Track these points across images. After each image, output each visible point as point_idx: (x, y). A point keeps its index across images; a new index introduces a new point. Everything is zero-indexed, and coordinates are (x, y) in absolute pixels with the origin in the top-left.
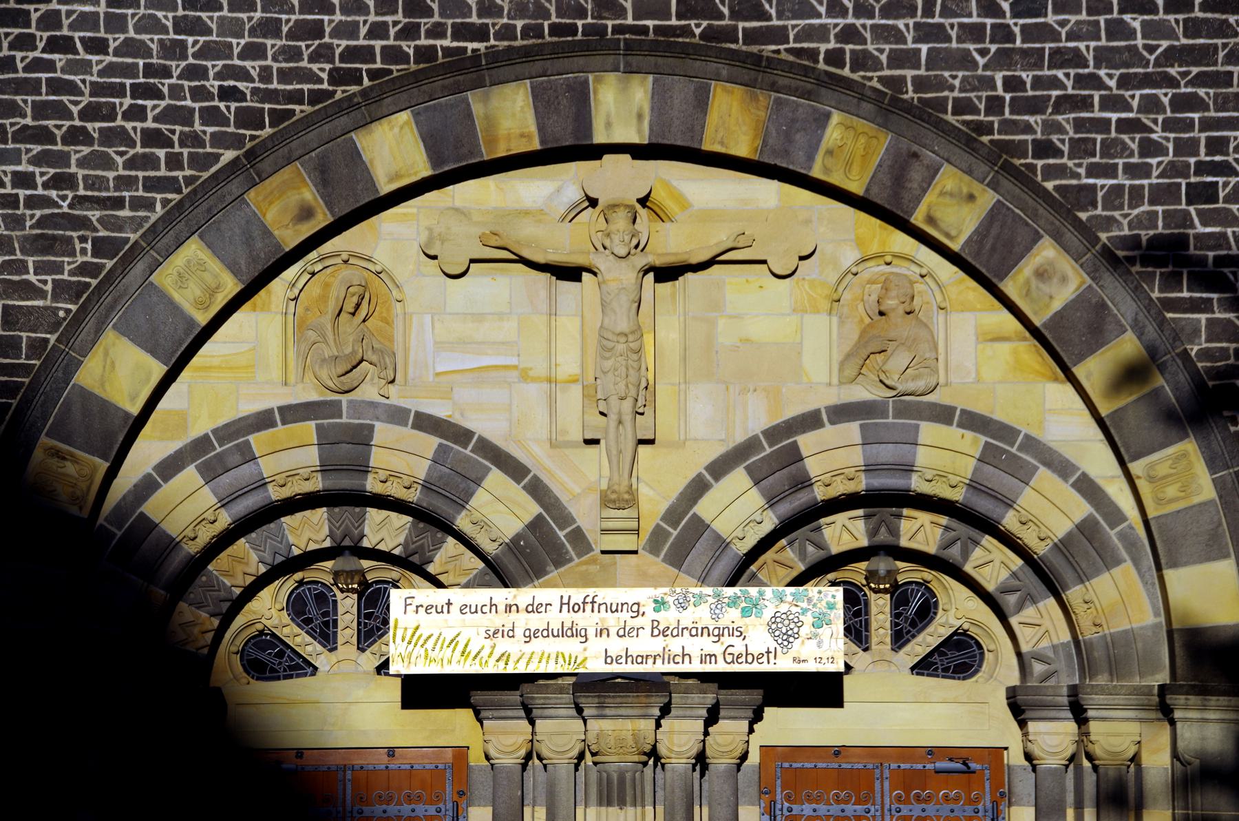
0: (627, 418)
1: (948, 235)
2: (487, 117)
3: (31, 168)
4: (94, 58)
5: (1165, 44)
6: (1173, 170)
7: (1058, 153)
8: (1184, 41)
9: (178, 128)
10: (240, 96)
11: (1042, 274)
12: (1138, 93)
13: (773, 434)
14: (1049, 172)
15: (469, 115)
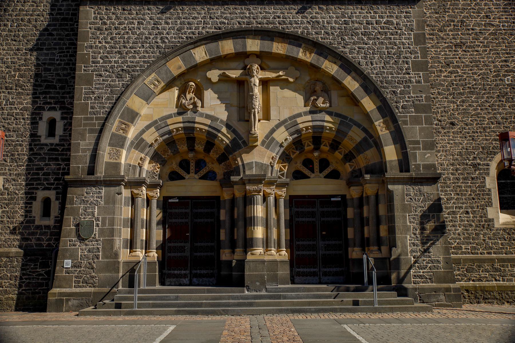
13: (290, 118)
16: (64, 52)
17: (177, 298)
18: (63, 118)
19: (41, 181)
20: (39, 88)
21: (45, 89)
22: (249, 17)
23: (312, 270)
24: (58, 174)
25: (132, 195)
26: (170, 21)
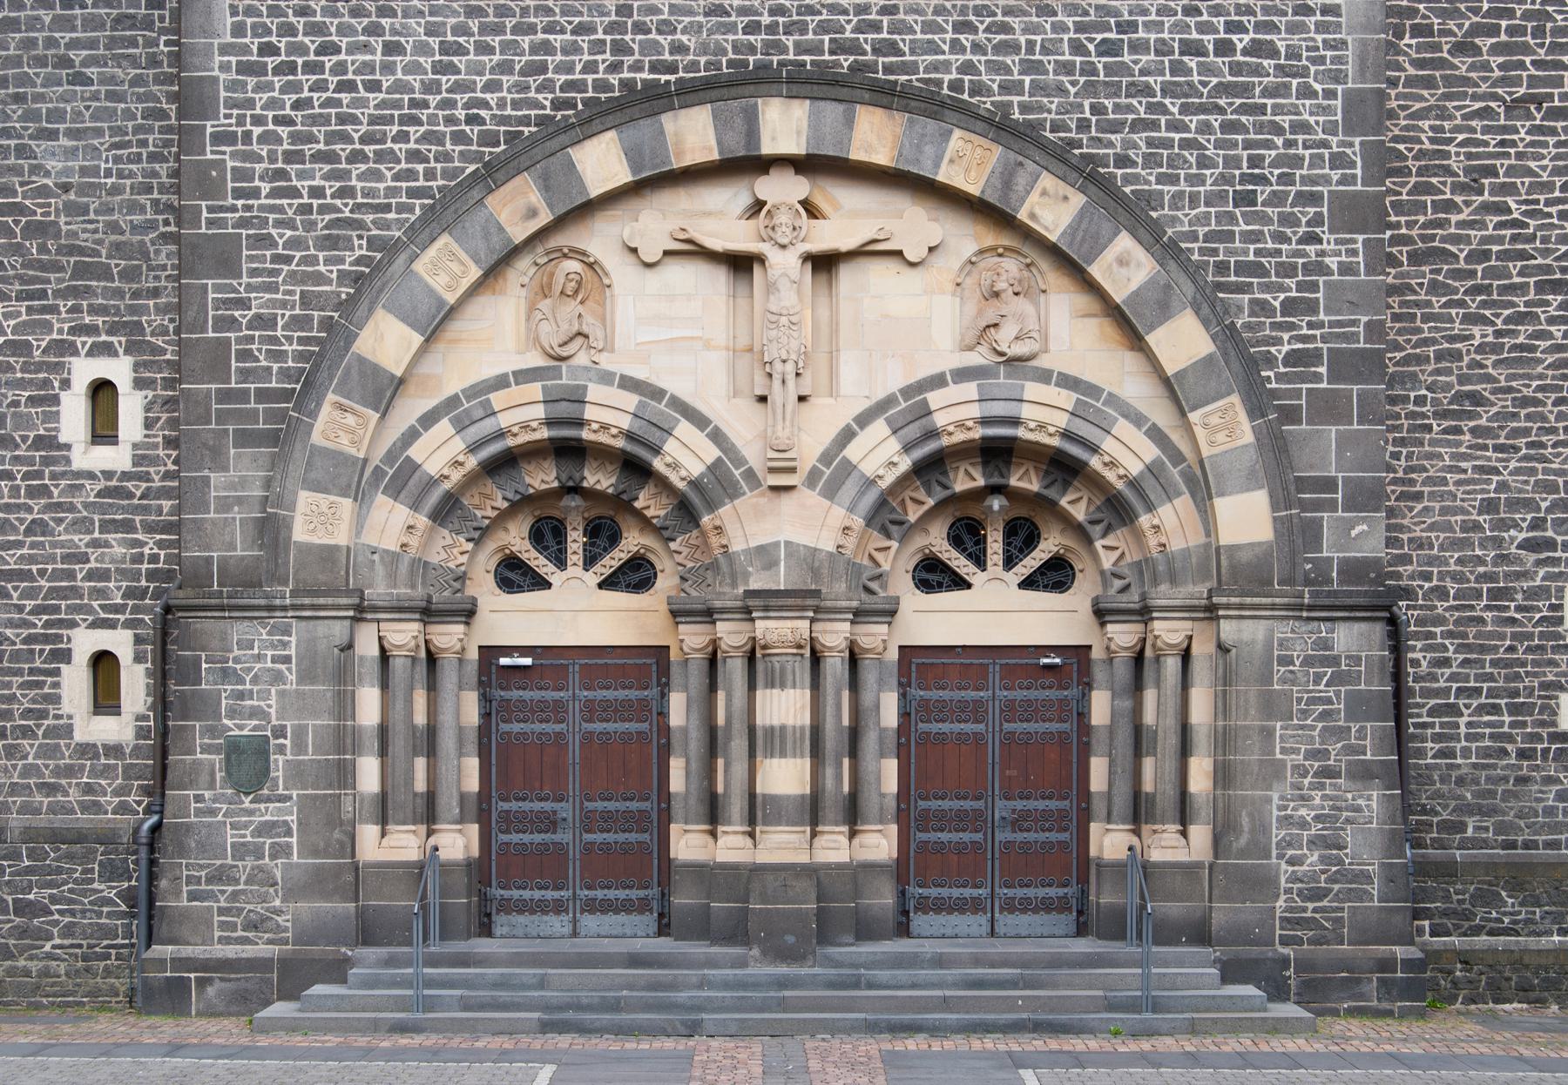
0: (791, 378)
1: (1046, 229)
2: (676, 134)
3: (323, 183)
4: (371, 96)
5: (1215, 81)
6: (1224, 179)
7: (1134, 164)
8: (1230, 78)
9: (434, 148)
10: (482, 122)
11: (1122, 262)
12: (1195, 118)
13: (907, 392)
14: (1127, 179)
15: (662, 132)
16: (128, 144)
17: (542, 984)
18: (139, 384)
19: (81, 597)
20: (52, 276)
21: (72, 278)
22: (772, 28)
23: (968, 892)
24: (136, 576)
25: (383, 649)
26: (495, 41)
